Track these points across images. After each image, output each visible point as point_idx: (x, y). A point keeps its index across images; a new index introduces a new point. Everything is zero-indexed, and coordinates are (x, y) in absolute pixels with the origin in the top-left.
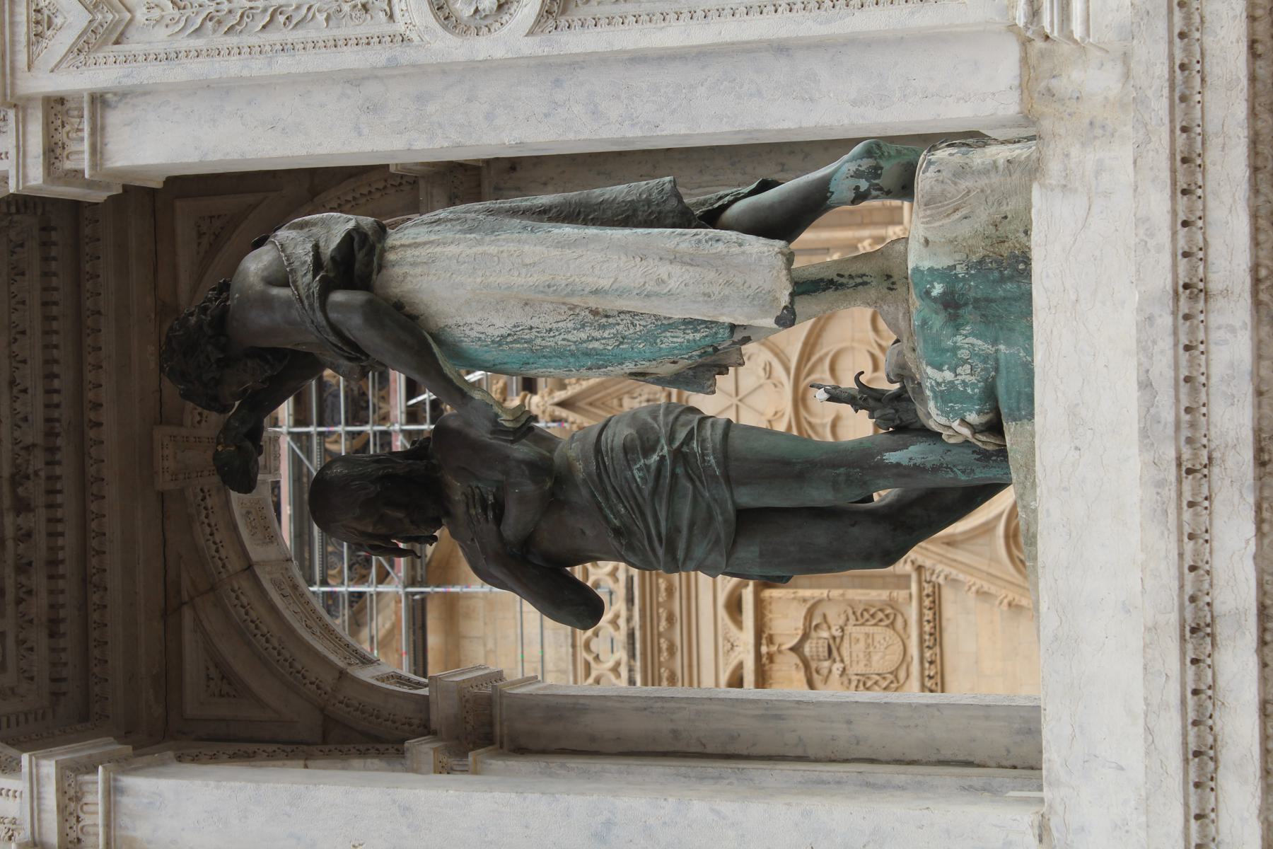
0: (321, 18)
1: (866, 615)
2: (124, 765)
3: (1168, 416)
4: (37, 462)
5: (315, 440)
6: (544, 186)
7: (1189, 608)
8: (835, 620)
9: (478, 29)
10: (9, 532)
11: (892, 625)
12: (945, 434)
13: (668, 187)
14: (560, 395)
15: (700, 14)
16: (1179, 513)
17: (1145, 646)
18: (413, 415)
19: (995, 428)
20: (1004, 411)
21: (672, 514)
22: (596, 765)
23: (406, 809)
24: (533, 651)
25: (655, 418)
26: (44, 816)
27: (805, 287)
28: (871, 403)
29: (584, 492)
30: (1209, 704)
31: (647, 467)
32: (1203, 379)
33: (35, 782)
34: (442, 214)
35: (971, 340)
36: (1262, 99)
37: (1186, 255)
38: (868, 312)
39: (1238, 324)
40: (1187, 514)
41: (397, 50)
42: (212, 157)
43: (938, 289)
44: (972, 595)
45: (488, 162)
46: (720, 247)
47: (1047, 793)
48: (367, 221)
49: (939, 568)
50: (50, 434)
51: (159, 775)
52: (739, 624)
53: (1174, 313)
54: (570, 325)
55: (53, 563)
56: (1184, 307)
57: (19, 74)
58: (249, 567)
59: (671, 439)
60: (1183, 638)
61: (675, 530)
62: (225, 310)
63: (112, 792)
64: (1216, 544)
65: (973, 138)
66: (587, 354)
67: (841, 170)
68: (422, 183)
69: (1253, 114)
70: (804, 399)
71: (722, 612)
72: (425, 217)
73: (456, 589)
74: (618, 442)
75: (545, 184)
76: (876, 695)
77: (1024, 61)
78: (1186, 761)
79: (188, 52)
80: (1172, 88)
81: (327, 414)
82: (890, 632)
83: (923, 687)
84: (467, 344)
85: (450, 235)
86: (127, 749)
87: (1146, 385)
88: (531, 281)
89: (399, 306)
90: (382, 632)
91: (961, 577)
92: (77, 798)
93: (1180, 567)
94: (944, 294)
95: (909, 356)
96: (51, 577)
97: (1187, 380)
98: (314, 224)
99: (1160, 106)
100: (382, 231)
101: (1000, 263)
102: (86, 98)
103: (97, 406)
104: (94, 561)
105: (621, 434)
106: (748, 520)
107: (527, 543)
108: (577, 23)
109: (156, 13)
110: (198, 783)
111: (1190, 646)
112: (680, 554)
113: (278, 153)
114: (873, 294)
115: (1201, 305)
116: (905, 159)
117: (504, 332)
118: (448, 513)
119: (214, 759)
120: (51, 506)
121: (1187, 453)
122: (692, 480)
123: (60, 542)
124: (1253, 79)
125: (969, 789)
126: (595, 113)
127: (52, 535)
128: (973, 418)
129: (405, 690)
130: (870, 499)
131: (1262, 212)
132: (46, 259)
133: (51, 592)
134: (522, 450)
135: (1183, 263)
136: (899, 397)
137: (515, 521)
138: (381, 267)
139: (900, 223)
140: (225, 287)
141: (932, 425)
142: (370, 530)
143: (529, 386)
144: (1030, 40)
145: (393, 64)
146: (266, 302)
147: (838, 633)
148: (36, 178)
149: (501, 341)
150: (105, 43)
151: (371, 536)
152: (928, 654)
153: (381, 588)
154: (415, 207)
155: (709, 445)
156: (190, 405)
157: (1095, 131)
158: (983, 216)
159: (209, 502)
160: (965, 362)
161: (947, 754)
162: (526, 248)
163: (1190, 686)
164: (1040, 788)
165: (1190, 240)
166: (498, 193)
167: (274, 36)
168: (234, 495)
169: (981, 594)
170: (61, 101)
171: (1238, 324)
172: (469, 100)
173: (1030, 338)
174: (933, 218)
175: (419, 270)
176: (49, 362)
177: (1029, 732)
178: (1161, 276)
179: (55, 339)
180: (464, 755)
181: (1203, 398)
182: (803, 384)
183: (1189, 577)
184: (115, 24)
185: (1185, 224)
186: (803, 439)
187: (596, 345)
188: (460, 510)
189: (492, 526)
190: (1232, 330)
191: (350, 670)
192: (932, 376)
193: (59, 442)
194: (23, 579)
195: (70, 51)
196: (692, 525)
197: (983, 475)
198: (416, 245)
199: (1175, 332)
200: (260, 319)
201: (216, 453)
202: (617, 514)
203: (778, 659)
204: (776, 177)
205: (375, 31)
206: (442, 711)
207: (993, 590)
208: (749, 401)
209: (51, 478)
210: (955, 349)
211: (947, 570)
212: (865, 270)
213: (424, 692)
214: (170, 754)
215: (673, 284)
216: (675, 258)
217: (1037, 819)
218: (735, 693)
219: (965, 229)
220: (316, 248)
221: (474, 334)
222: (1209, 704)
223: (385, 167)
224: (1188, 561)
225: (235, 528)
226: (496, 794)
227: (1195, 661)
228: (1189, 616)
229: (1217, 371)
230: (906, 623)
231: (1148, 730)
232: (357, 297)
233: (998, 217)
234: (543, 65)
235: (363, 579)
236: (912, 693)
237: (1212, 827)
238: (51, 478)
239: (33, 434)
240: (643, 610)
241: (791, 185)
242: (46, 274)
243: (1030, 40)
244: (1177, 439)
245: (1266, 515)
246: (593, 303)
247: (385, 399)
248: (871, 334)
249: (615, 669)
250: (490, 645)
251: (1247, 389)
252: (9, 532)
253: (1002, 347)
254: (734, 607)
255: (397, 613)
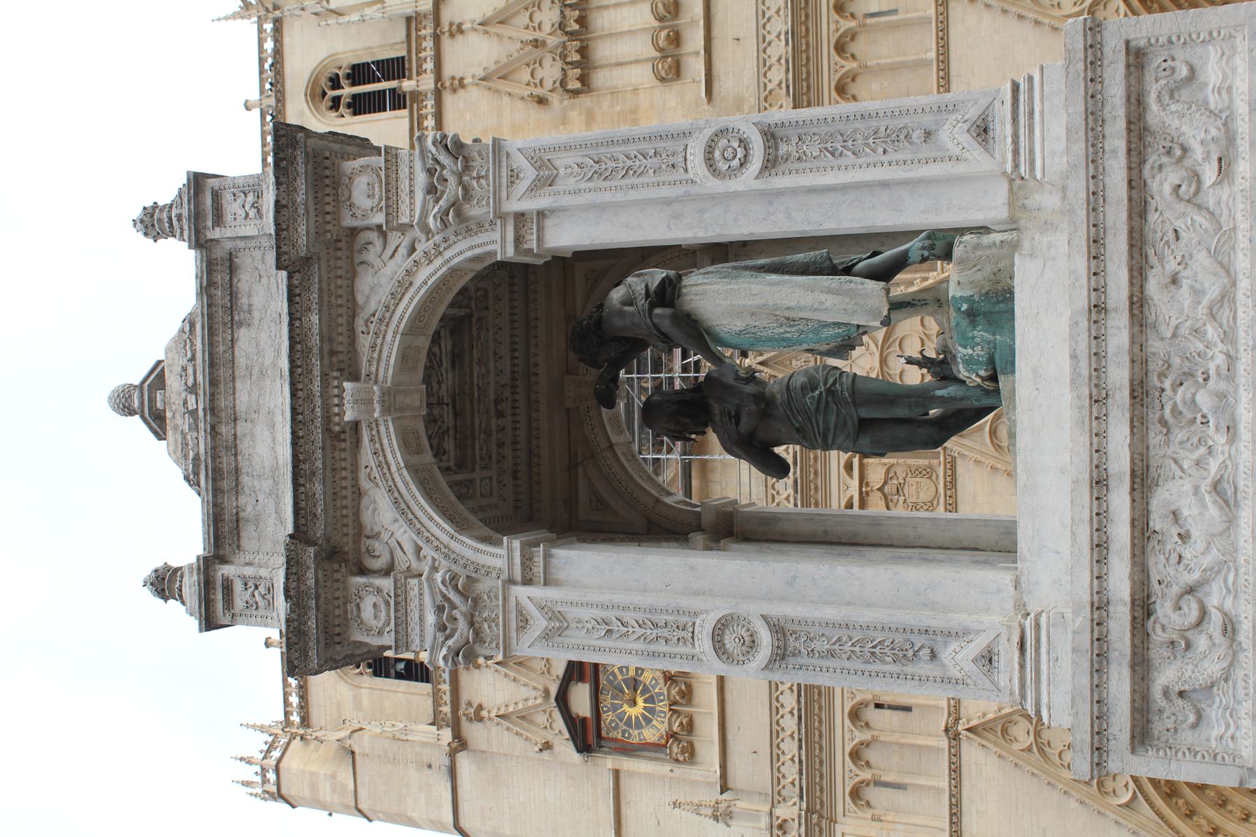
0: (651, 171)
1: (917, 472)
2: (553, 543)
3: (1085, 372)
4: (507, 393)
5: (636, 381)
6: (761, 254)
7: (1095, 471)
8: (901, 475)
9: (730, 176)
10: (494, 427)
11: (930, 478)
12: (968, 381)
13: (825, 255)
14: (760, 359)
15: (843, 167)
16: (1091, 423)
17: (1072, 490)
18: (685, 369)
19: (994, 378)
20: (998, 369)
21: (826, 421)
22: (785, 547)
23: (692, 568)
24: (745, 489)
25: (817, 372)
26: (515, 567)
27: (898, 306)
28: (929, 365)
29: (781, 410)
30: (1105, 520)
31: (813, 397)
32: (1104, 354)
33: (510, 551)
34: (710, 269)
35: (981, 333)
36: (1135, 210)
37: (1095, 290)
38: (919, 317)
39: (1122, 326)
40: (1095, 423)
41: (690, 186)
42: (596, 242)
43: (964, 307)
44: (972, 462)
45: (732, 243)
46: (852, 285)
47: (1019, 565)
48: (672, 273)
49: (955, 448)
50: (514, 379)
51: (569, 549)
52: (851, 476)
53: (1089, 320)
54: (775, 325)
55: (515, 443)
56: (1094, 317)
57: (503, 202)
58: (611, 446)
59: (825, 383)
60: (1091, 487)
61: (827, 430)
62: (601, 317)
63: (547, 556)
64: (1109, 439)
65: (983, 230)
66: (783, 340)
67: (914, 245)
68: (698, 254)
69: (1130, 218)
70: (885, 361)
71: (842, 470)
72: (702, 271)
73: (707, 457)
74: (799, 384)
75: (761, 253)
76: (922, 514)
77: (1011, 190)
78: (1092, 549)
79: (585, 190)
80: (1088, 204)
81: (642, 368)
82: (929, 481)
83: (946, 510)
84: (722, 335)
85: (714, 280)
86: (554, 536)
87: (1074, 357)
88: (755, 303)
89: (688, 315)
90: (669, 479)
91: (966, 453)
92: (530, 559)
93: (1091, 451)
94: (968, 309)
95: (949, 341)
96: (514, 450)
97: (1095, 354)
98: (646, 274)
99: (1082, 214)
100: (679, 277)
101: (997, 294)
102: (535, 213)
103: (536, 365)
104: (534, 442)
105: (800, 380)
106: (865, 425)
107: (752, 435)
108: (781, 173)
109: (569, 171)
110: (589, 553)
111: (1095, 491)
112: (830, 442)
113: (630, 240)
114: (930, 309)
115: (1103, 316)
116: (947, 240)
117: (742, 328)
118: (711, 420)
119: (594, 541)
120: (514, 415)
121: (1095, 392)
122: (836, 404)
123: (518, 432)
124: (1130, 199)
125: (977, 562)
126: (789, 218)
127: (515, 429)
128: (982, 373)
129: (688, 508)
130: (928, 414)
131: (1135, 268)
132: (512, 292)
133: (514, 457)
134: (750, 389)
135: (1093, 294)
136: (943, 362)
137: (745, 424)
138: (679, 296)
139: (936, 270)
140: (601, 306)
141: (961, 377)
142: (672, 428)
143: (744, 354)
144: (1014, 180)
145: (687, 194)
146: (622, 314)
147: (902, 482)
148: (510, 252)
149: (739, 333)
150: (544, 185)
151: (674, 431)
152: (948, 493)
153: (669, 456)
154: (695, 265)
155: (845, 386)
156: (582, 364)
157: (1047, 226)
158: (988, 270)
159: (591, 413)
160: (979, 344)
161: (966, 544)
162: (753, 286)
163: (1095, 511)
164: (1015, 562)
165: (1097, 283)
166: (737, 258)
167: (628, 181)
168: (604, 410)
169: (977, 462)
170: (523, 214)
171: (1122, 326)
172: (725, 212)
173: (1013, 331)
174: (962, 271)
175: (698, 297)
176: (513, 343)
177: (1008, 533)
178: (1082, 301)
179: (516, 332)
180: (718, 541)
181: (1104, 364)
182: (885, 354)
183: (1095, 455)
184: (549, 176)
185: (1095, 274)
186: (885, 381)
187: (788, 335)
188: (717, 419)
189: (734, 426)
190: (1119, 328)
191: (661, 498)
192: (962, 352)
193: (518, 383)
194: (500, 451)
195: (527, 190)
196: (836, 427)
197: (986, 402)
198: (697, 285)
199: (1089, 330)
200: (618, 322)
201: (596, 389)
202: (798, 421)
203: (871, 494)
204: (878, 249)
205: (678, 178)
206: (707, 519)
207: (983, 460)
208: (856, 362)
209: (514, 401)
210: (973, 338)
211: (959, 449)
212: (927, 297)
213: (698, 509)
214: (575, 538)
215: (828, 304)
216: (829, 291)
217: (1014, 577)
218: (849, 512)
219: (979, 276)
220: (647, 286)
221: (726, 330)
222: (1105, 520)
223: (680, 246)
224: (1095, 447)
225: (604, 426)
226: (738, 562)
227: (1097, 499)
228: (1095, 476)
229: (1111, 349)
230: (937, 476)
231: (1073, 533)
232: (667, 311)
233: (996, 270)
234: (763, 194)
235: (659, 452)
236: (940, 512)
237: (1105, 583)
238: (514, 401)
239: (505, 379)
240: (801, 469)
241: (888, 254)
242: (511, 300)
243: (1014, 180)
244: (1090, 385)
245: (1136, 424)
246: (787, 314)
247: (671, 360)
248: (921, 328)
249: (787, 499)
250: (724, 485)
251: (1127, 359)
252: (494, 427)
253: (998, 337)
254: (849, 467)
255: (677, 469)
